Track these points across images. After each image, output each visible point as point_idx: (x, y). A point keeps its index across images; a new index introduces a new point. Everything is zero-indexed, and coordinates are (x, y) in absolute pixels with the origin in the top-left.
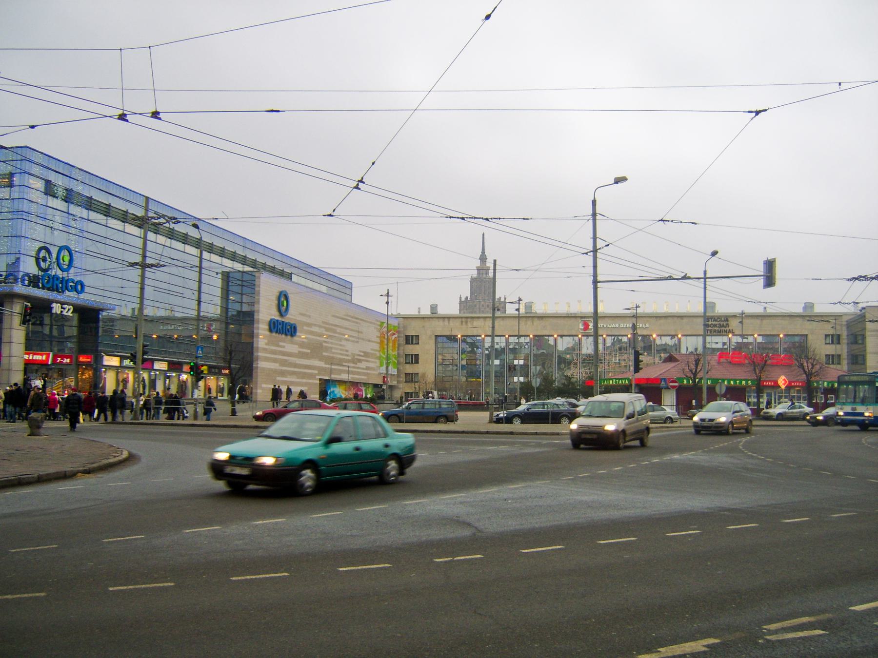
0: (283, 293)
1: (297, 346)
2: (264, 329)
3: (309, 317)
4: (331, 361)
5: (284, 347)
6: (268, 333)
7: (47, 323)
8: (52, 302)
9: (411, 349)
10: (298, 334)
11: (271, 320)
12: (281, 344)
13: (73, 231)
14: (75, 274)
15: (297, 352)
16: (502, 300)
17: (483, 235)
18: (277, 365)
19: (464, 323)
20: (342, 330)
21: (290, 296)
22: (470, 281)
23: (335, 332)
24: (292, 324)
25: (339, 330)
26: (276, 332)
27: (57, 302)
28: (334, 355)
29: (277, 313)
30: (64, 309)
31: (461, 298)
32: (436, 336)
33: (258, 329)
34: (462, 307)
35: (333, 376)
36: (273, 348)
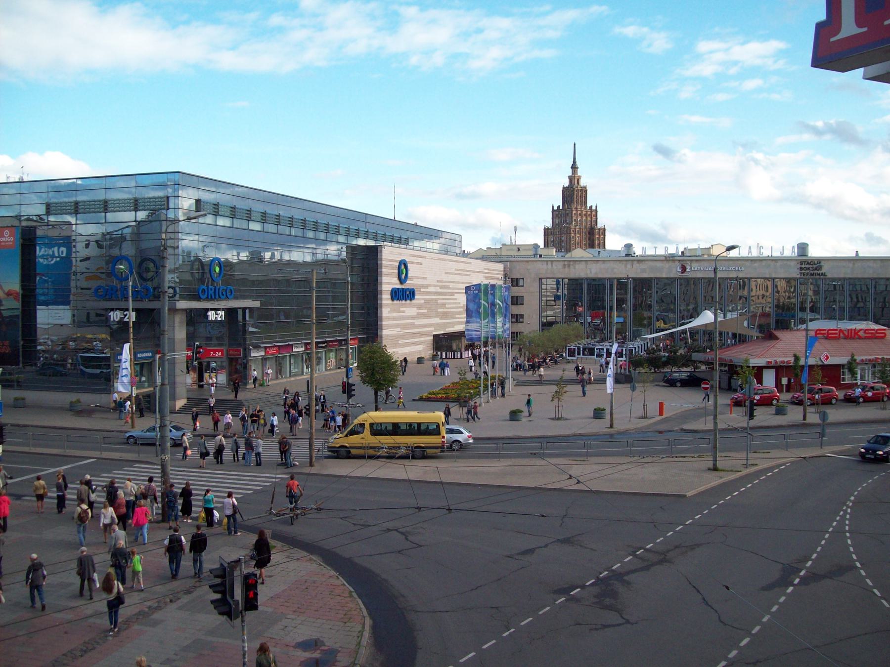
0: (403, 262)
1: (416, 309)
2: (387, 299)
3: (425, 278)
4: (445, 315)
5: (403, 312)
6: (390, 302)
7: (218, 379)
8: (207, 310)
9: (516, 291)
10: (416, 297)
11: (393, 289)
12: (402, 309)
13: (261, 392)
14: (216, 240)
15: (416, 314)
16: (594, 208)
17: (575, 144)
18: (399, 329)
19: (566, 266)
20: (454, 284)
21: (409, 266)
22: (563, 191)
23: (448, 288)
24: (411, 289)
25: (451, 285)
26: (398, 300)
27: (212, 309)
28: (449, 310)
29: (398, 282)
30: (217, 314)
31: (553, 207)
32: (540, 278)
33: (381, 299)
34: (555, 216)
35: (447, 330)
36: (395, 315)
